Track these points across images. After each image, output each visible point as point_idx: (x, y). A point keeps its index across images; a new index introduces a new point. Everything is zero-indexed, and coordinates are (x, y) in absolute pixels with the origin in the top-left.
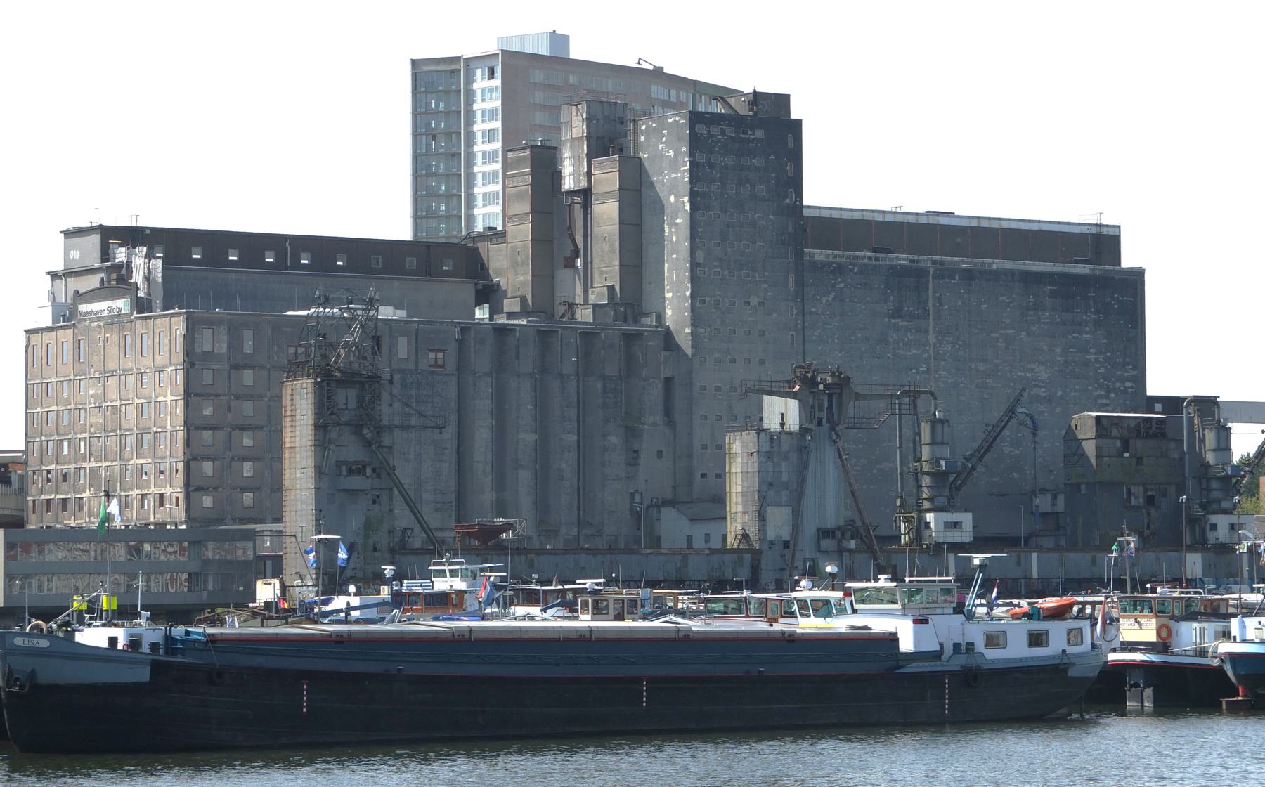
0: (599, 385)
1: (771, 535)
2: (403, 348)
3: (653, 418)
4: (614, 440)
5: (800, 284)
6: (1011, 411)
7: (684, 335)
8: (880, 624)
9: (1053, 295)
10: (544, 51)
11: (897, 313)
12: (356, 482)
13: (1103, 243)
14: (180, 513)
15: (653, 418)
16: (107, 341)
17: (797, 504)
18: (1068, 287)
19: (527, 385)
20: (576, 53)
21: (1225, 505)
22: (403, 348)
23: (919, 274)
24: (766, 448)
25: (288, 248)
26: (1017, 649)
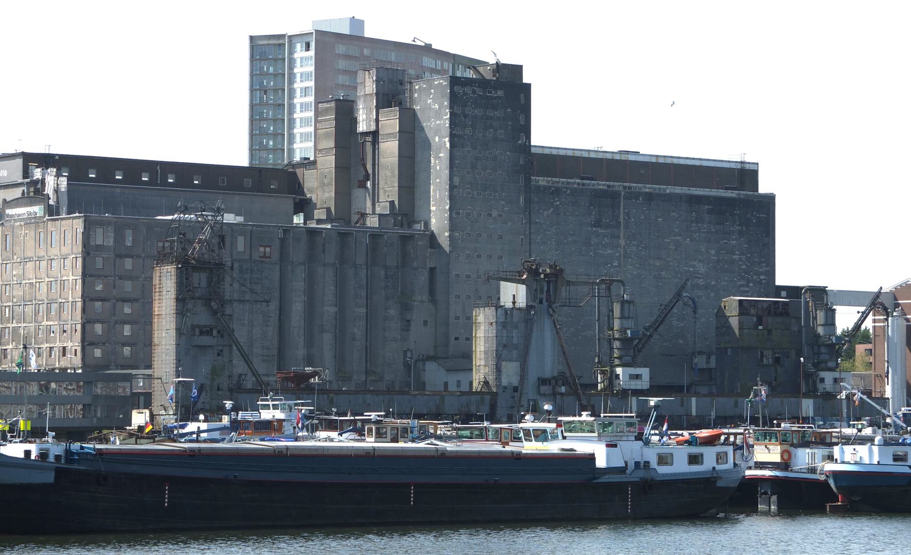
0: (382, 272)
1: (505, 382)
2: (241, 244)
3: (421, 296)
4: (392, 312)
5: (528, 201)
6: (678, 295)
7: (444, 237)
8: (582, 447)
9: (710, 212)
10: (346, 31)
11: (598, 224)
12: (205, 340)
13: (746, 175)
14: (77, 361)
15: (421, 296)
16: (27, 236)
17: (524, 362)
18: (721, 207)
19: (330, 272)
20: (369, 33)
21: (831, 364)
22: (241, 244)
23: (612, 196)
24: (502, 319)
25: (159, 171)
26: (680, 466)
